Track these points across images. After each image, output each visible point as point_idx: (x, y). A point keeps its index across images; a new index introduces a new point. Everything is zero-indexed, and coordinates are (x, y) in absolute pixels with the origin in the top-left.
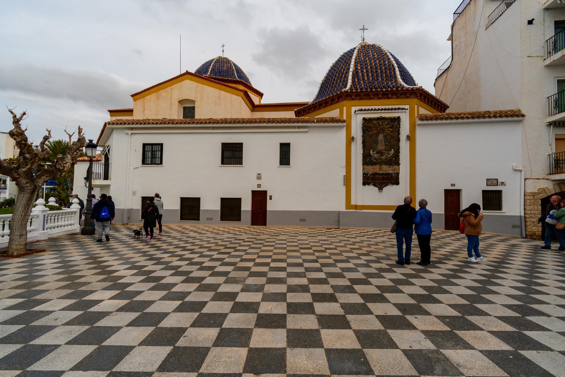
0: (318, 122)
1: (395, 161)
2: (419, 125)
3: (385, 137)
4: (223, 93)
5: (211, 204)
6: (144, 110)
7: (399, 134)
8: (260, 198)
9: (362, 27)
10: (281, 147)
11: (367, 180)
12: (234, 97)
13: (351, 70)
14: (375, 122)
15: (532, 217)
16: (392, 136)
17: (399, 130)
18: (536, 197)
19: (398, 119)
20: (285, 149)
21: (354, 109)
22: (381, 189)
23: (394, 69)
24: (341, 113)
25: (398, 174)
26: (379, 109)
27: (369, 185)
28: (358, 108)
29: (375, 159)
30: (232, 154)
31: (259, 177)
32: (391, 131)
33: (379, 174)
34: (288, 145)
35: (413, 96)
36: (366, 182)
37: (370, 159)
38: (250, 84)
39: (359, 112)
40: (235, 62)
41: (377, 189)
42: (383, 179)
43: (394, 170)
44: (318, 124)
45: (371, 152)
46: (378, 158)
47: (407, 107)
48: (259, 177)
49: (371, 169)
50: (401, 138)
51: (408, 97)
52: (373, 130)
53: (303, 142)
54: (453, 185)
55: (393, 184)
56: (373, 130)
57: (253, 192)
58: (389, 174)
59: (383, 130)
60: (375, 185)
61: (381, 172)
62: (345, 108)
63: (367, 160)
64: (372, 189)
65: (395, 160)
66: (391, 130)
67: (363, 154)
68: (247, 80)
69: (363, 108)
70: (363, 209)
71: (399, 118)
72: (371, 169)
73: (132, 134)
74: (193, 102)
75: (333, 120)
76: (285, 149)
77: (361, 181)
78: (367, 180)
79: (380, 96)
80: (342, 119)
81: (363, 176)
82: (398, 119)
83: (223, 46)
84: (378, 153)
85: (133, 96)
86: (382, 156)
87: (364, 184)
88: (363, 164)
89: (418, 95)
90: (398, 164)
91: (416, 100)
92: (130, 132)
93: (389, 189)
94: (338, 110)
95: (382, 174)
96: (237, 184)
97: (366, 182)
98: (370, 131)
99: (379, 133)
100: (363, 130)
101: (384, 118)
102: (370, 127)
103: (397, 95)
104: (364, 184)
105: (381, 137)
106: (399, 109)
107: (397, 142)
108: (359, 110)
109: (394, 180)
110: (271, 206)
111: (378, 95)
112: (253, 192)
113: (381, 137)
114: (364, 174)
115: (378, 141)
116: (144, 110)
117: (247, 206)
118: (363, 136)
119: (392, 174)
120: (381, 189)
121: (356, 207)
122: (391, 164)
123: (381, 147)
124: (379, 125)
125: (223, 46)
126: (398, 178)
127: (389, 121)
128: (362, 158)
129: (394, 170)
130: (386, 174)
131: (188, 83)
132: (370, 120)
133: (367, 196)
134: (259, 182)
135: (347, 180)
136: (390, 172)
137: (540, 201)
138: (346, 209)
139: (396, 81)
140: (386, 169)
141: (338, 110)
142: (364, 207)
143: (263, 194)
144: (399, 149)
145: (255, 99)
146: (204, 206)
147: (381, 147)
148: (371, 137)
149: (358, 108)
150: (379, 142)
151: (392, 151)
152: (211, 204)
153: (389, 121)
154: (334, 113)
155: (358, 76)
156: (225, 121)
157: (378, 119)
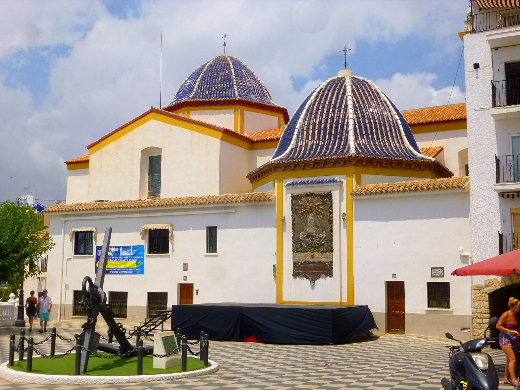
4: (196, 134)
6: (101, 166)
12: (211, 138)
14: (304, 199)
15: (477, 317)
16: (323, 216)
18: (482, 291)
19: (329, 196)
20: (212, 234)
22: (313, 281)
25: (332, 262)
28: (290, 182)
31: (185, 267)
32: (323, 210)
33: (311, 263)
37: (301, 244)
42: (315, 268)
43: (327, 257)
48: (185, 267)
52: (302, 209)
54: (394, 276)
55: (327, 275)
56: (302, 209)
60: (306, 276)
64: (305, 282)
65: (328, 245)
66: (321, 207)
73: (65, 221)
74: (160, 150)
76: (212, 234)
83: (225, 36)
88: (294, 252)
90: (332, 251)
92: (64, 219)
93: (322, 282)
109: (326, 270)
113: (311, 217)
114: (294, 263)
116: (101, 166)
120: (313, 281)
123: (311, 230)
125: (225, 36)
128: (292, 243)
129: (327, 257)
134: (185, 273)
135: (277, 270)
136: (323, 260)
137: (487, 296)
140: (319, 257)
146: (131, 302)
157: (307, 195)
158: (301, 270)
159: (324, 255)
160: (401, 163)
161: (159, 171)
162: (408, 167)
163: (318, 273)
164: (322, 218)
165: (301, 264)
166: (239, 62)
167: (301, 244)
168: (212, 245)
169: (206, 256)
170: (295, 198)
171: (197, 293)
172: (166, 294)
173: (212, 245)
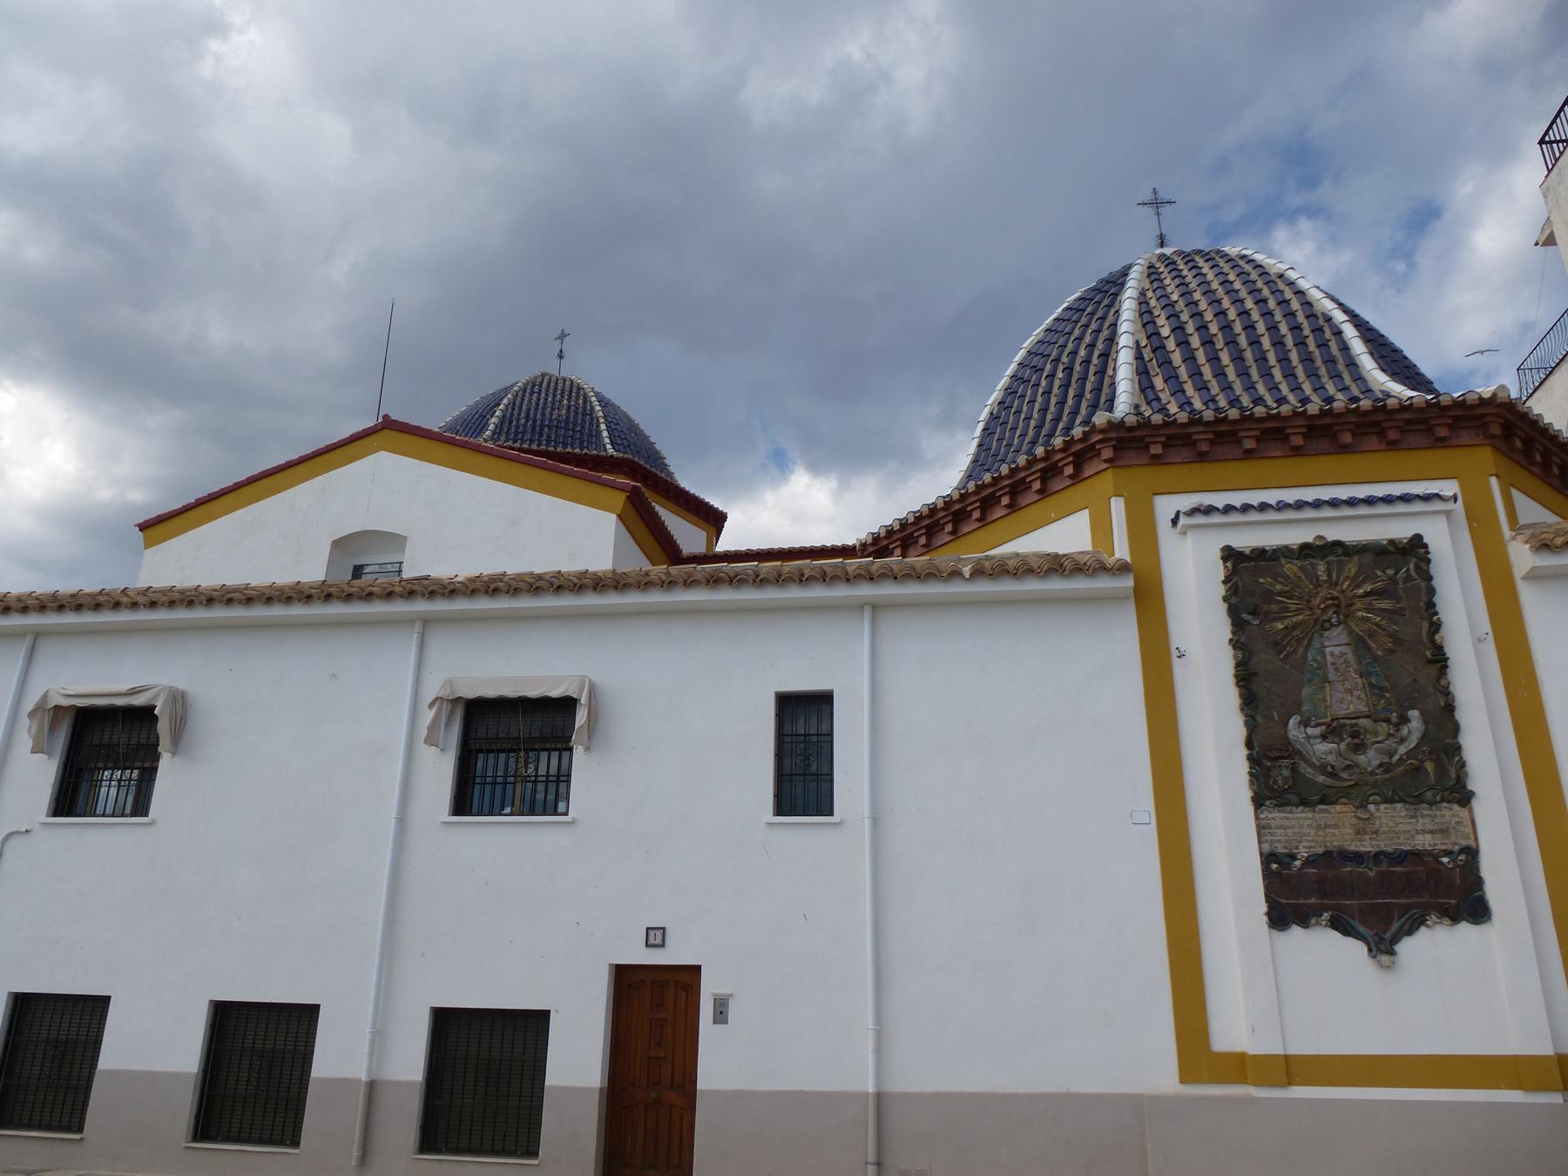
0: (978, 572)
1: (1439, 775)
2: (1534, 576)
3: (1359, 644)
5: (369, 1049)
7: (1436, 627)
8: (656, 1008)
9: (1148, 197)
10: (780, 715)
11: (1294, 895)
13: (1124, 340)
14: (1291, 568)
17: (1431, 605)
20: (803, 723)
21: (1166, 506)
22: (1382, 946)
23: (1338, 333)
24: (1101, 528)
25: (1472, 853)
26: (1289, 512)
27: (1305, 924)
29: (1323, 768)
30: (511, 753)
33: (1358, 857)
34: (822, 702)
35: (1465, 437)
36: (1284, 911)
37: (1294, 769)
38: (670, 474)
39: (1199, 519)
40: (609, 395)
41: (1355, 949)
44: (984, 587)
45: (1294, 729)
46: (1339, 764)
47: (1449, 488)
49: (1309, 832)
50: (1450, 651)
51: (1440, 443)
53: (910, 687)
55: (1455, 918)
56: (1286, 610)
57: (622, 974)
58: (1417, 855)
59: (1342, 609)
60: (1342, 926)
61: (1367, 846)
62: (1117, 507)
63: (1275, 777)
64: (1326, 951)
65: (1442, 772)
66: (1386, 604)
67: (1249, 744)
68: (657, 458)
69: (1219, 500)
70: (1290, 1082)
71: (1417, 543)
72: (1309, 832)
75: (1056, 565)
76: (803, 723)
77: (1259, 905)
78: (1294, 895)
79: (1297, 441)
80: (1110, 561)
81: (1267, 874)
82: (1416, 548)
83: (562, 337)
84: (1332, 731)
85: (144, 527)
86: (1359, 748)
87: (1280, 918)
88: (1258, 802)
89: (1496, 430)
90: (1464, 797)
91: (1485, 457)
93: (1433, 947)
94: (1083, 517)
95: (1378, 856)
96: (535, 926)
97: (1284, 911)
98: (1268, 618)
99: (1325, 626)
100: (1233, 612)
101: (1338, 544)
102: (1268, 596)
103: (1381, 434)
104: (1280, 918)
105: (1335, 645)
106: (1406, 498)
107: (1433, 671)
108: (1194, 511)
110: (722, 1062)
111: (1286, 438)
112: (622, 974)
113: (1335, 645)
114: (1268, 858)
115: (1322, 666)
117: (577, 1061)
118: (1235, 644)
119: (1435, 856)
120: (1382, 946)
121: (1239, 1067)
122: (1419, 800)
124: (1318, 585)
125: (562, 337)
126: (1479, 882)
127: (1368, 558)
128: (1244, 767)
129: (1444, 832)
130: (1401, 857)
131: (385, 468)
132: (1260, 554)
133: (1304, 991)
136: (1424, 842)
138: (1185, 1078)
139: (1359, 378)
140: (1399, 828)
141: (1083, 517)
142: (1290, 1069)
143: (681, 983)
144: (1450, 708)
145: (688, 536)
146: (336, 1057)
147: (1347, 699)
148: (1277, 646)
149: (1186, 502)
150: (1332, 676)
151: (1415, 723)
152: (369, 1049)
153: (1368, 558)
154: (1067, 534)
155: (1166, 363)
156: (491, 586)
157: (1306, 551)
158: (1298, 893)
159: (1423, 823)
160: (1329, 427)
161: (406, 425)
162: (1373, 442)
163: (1405, 909)
164: (1391, 651)
165: (1309, 862)
166: (633, 428)
167: (1294, 769)
168: (803, 782)
169: (769, 824)
170: (1242, 567)
171: (721, 1015)
172: (539, 1019)
173: (803, 782)
